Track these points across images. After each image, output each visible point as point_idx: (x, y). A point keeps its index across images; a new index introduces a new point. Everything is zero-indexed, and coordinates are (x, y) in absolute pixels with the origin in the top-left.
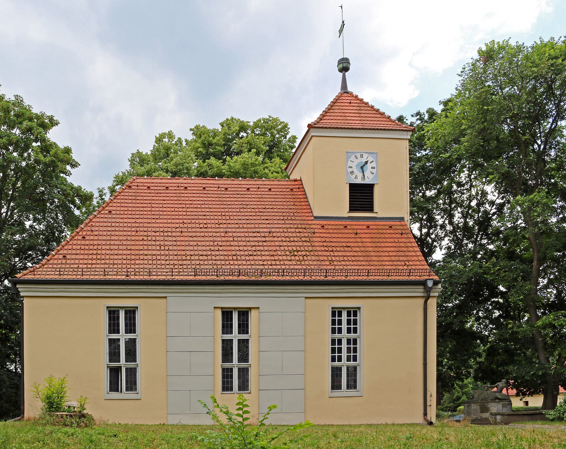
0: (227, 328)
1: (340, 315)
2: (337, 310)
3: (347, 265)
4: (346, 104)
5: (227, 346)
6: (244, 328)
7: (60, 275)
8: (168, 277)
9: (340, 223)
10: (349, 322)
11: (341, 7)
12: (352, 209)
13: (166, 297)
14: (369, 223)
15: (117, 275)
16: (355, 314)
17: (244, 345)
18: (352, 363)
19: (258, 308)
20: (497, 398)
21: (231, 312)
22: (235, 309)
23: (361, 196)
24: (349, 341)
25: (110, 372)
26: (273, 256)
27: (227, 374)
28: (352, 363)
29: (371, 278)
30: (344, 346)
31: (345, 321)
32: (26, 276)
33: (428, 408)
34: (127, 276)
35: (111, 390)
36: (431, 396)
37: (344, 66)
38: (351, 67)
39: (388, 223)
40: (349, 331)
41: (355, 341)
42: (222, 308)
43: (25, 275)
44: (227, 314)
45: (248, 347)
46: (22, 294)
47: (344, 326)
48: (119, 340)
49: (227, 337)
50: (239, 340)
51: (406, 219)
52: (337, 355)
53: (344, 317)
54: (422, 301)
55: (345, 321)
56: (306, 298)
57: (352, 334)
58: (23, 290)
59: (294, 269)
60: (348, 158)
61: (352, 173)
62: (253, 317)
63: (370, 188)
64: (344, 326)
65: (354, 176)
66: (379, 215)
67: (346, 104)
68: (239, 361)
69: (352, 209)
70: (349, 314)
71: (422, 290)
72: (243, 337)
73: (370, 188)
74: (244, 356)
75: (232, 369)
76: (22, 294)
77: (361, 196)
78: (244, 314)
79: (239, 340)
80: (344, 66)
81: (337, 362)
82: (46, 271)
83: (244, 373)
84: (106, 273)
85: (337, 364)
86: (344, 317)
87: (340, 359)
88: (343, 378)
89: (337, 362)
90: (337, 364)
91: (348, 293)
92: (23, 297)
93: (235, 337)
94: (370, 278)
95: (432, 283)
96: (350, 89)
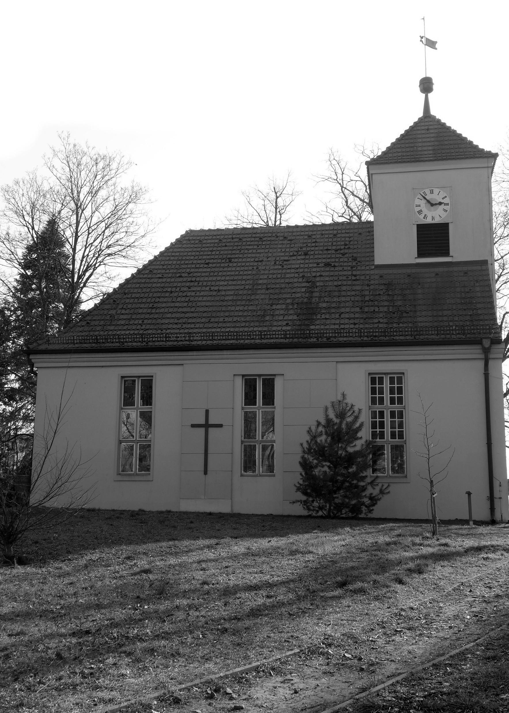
2: (377, 376)
3: (245, 327)
4: (423, 132)
10: (392, 391)
11: (423, 19)
15: (212, 340)
22: (260, 376)
29: (51, 347)
33: (496, 501)
36: (500, 486)
37: (426, 85)
38: (434, 87)
39: (432, 270)
40: (392, 401)
41: (401, 415)
42: (243, 376)
47: (387, 396)
53: (387, 385)
54: (481, 364)
56: (337, 362)
61: (420, 212)
64: (387, 396)
65: (423, 215)
69: (420, 254)
71: (480, 351)
78: (269, 383)
80: (426, 85)
81: (397, 440)
84: (263, 337)
86: (387, 385)
91: (161, 360)
93: (259, 408)
94: (263, 341)
95: (489, 342)
96: (433, 112)
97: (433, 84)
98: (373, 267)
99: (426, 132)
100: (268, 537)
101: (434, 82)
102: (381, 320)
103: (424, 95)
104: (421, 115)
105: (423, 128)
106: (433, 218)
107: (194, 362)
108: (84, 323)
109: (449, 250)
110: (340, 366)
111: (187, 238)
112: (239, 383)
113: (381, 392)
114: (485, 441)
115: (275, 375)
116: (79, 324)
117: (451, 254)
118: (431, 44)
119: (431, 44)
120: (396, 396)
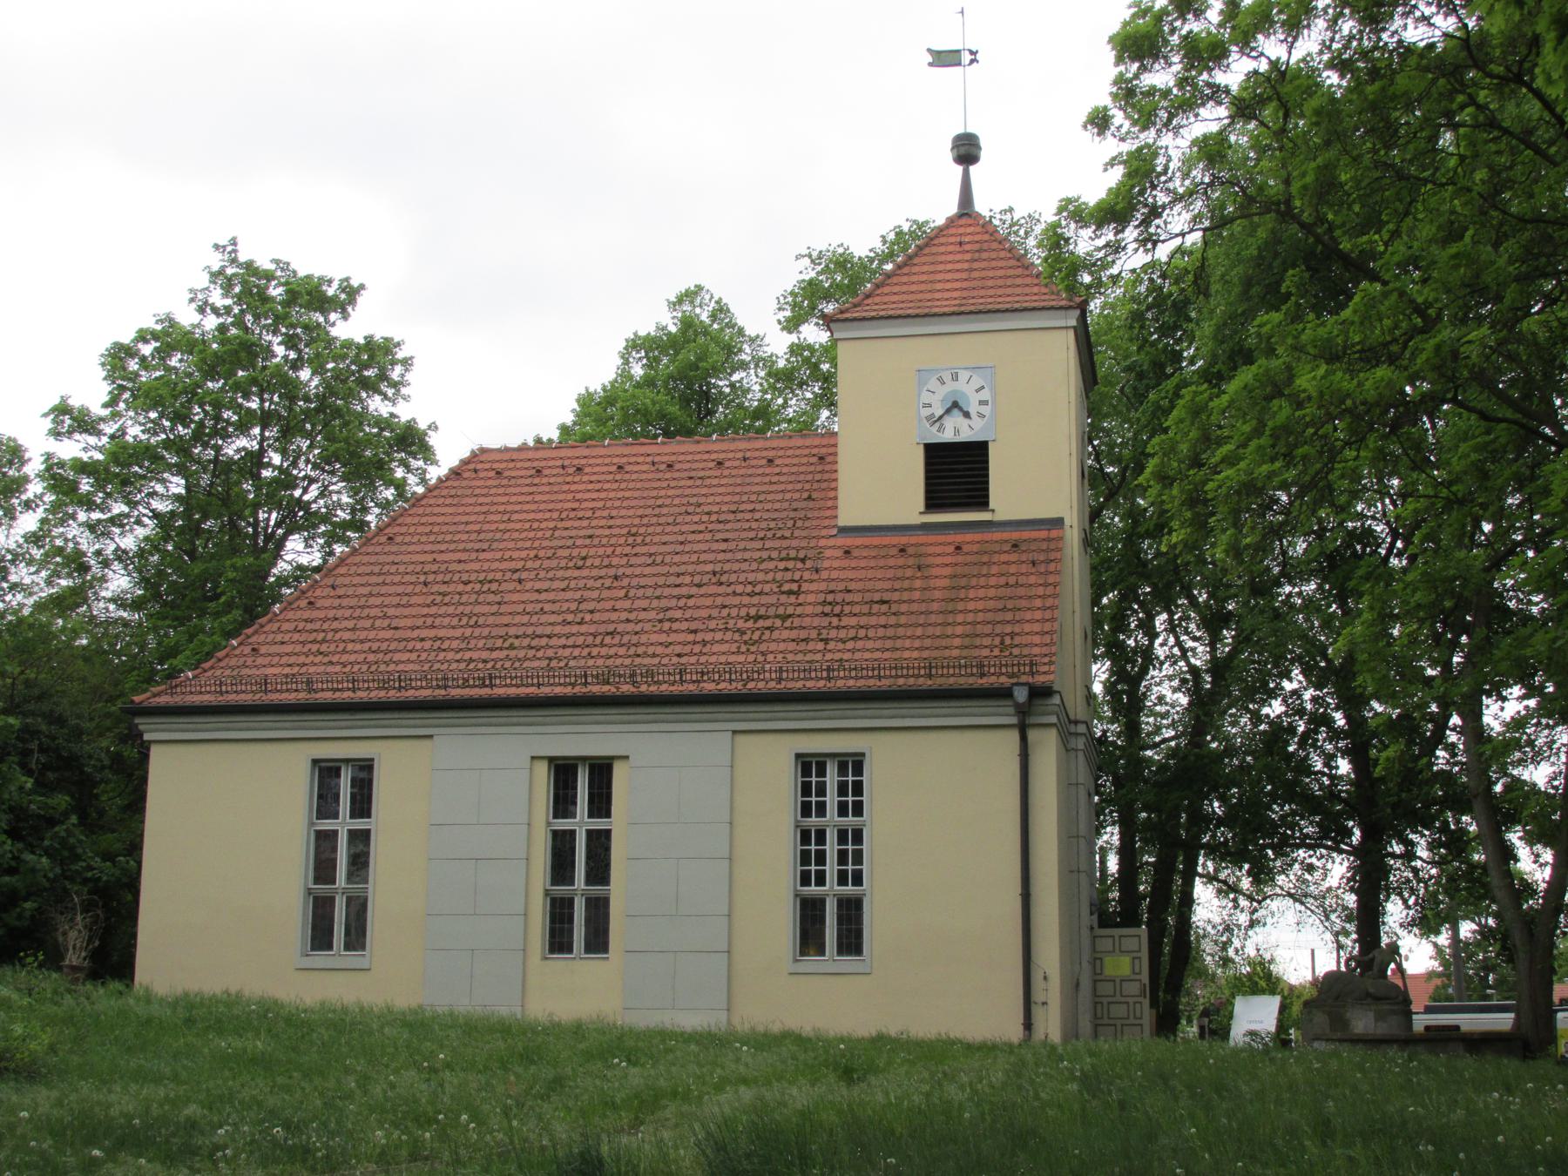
0: (563, 803)
1: (822, 772)
4: (951, 248)
5: (562, 845)
6: (601, 804)
7: (982, 675)
8: (577, 689)
9: (886, 541)
10: (842, 790)
12: (934, 501)
13: (431, 737)
14: (959, 538)
16: (859, 769)
17: (600, 843)
18: (850, 889)
19: (627, 757)
20: (1368, 995)
21: (338, 770)
23: (957, 472)
24: (842, 836)
25: (802, 909)
26: (695, 632)
27: (560, 912)
28: (850, 889)
30: (831, 847)
31: (829, 786)
32: (157, 699)
34: (829, 679)
35: (804, 951)
37: (967, 151)
38: (983, 155)
41: (858, 836)
42: (551, 760)
43: (155, 696)
44: (563, 771)
45: (608, 849)
46: (146, 737)
48: (335, 832)
49: (563, 824)
50: (589, 832)
51: (1067, 522)
52: (850, 867)
53: (832, 778)
54: (1014, 736)
55: (829, 786)
56: (734, 732)
57: (814, 819)
58: (152, 731)
59: (723, 660)
60: (921, 384)
62: (620, 778)
63: (978, 451)
66: (1000, 516)
67: (951, 248)
68: (589, 881)
70: (842, 769)
72: (599, 824)
73: (978, 451)
74: (599, 871)
75: (571, 901)
76: (146, 737)
77: (957, 472)
78: (602, 771)
79: (589, 832)
80: (967, 151)
81: (813, 888)
82: (197, 687)
83: (599, 910)
85: (813, 889)
86: (832, 778)
87: (821, 880)
88: (830, 923)
89: (813, 888)
90: (813, 889)
91: (903, 717)
92: (150, 742)
97: (980, 148)
98: (835, 531)
99: (958, 248)
100: (342, 1033)
101: (982, 144)
102: (618, 605)
103: (960, 169)
104: (953, 209)
105: (952, 240)
106: (957, 431)
107: (448, 730)
108: (247, 650)
109: (987, 496)
110: (740, 739)
111: (471, 466)
112: (542, 772)
113: (822, 791)
114: (1033, 898)
115: (613, 758)
116: (237, 652)
117: (992, 505)
118: (945, 58)
119: (945, 58)
120: (850, 799)
